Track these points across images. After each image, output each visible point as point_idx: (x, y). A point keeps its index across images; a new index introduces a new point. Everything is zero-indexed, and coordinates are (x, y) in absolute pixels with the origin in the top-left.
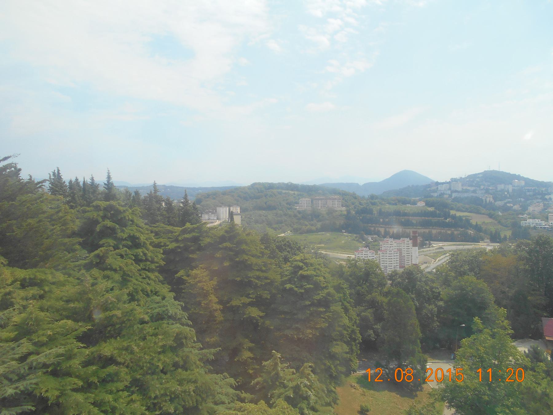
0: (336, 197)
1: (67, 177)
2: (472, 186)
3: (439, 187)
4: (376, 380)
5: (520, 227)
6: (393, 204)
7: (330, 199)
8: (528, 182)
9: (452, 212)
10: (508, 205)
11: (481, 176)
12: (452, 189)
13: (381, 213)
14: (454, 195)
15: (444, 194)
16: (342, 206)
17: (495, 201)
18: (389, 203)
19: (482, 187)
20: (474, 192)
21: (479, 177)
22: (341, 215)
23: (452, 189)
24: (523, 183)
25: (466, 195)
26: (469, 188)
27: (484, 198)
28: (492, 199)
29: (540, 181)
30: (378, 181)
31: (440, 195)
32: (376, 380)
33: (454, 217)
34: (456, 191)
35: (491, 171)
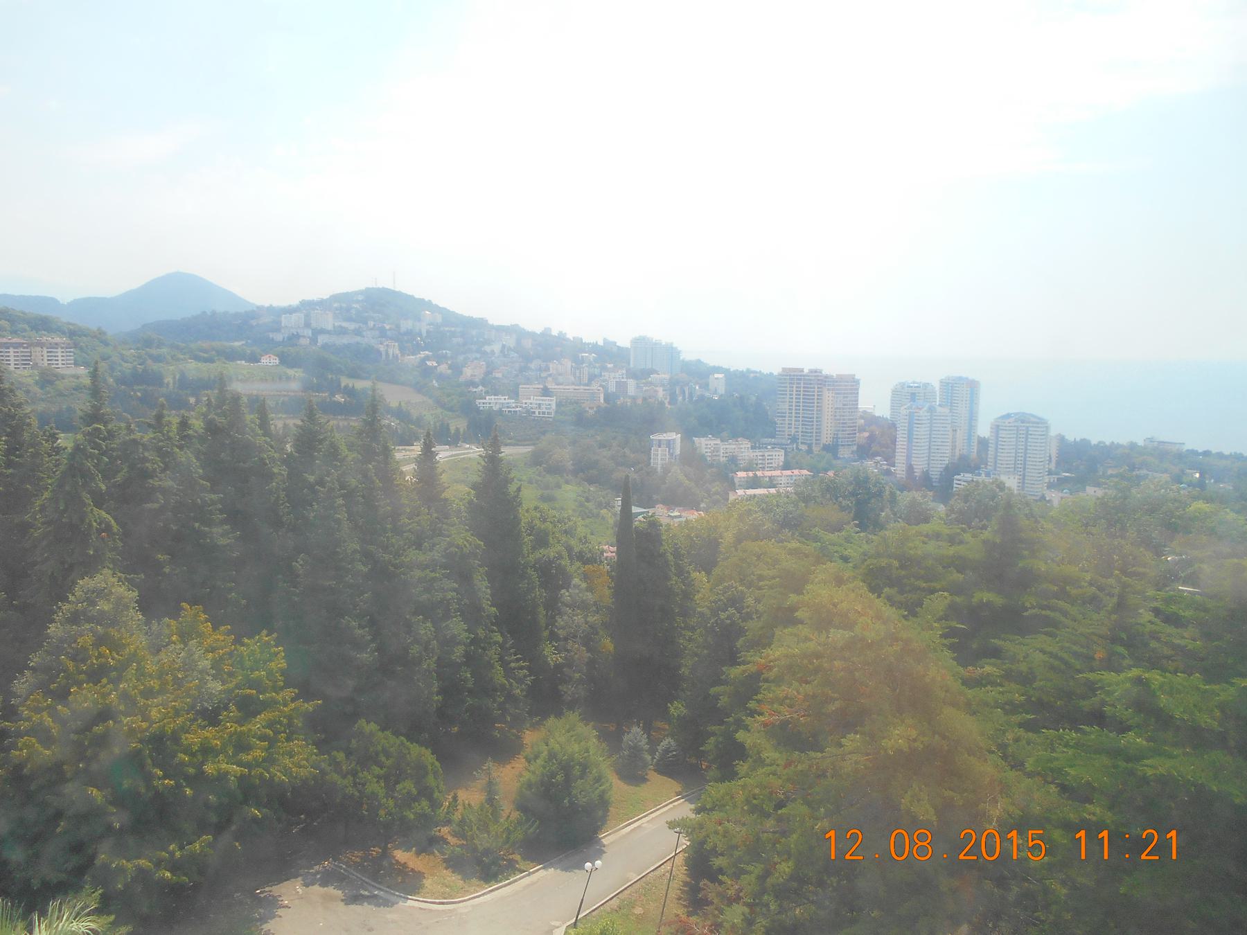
0: (57, 340)
1: (1070, 438)
2: (350, 320)
3: (284, 320)
4: (961, 857)
5: (478, 411)
6: (205, 360)
7: (41, 345)
8: (447, 315)
9: (345, 381)
10: (429, 363)
11: (360, 298)
12: (314, 325)
13: (183, 383)
14: (322, 339)
15: (298, 336)
16: (76, 364)
17: (403, 355)
18: (197, 358)
19: (371, 324)
20: (358, 332)
21: (358, 302)
22: (77, 388)
23: (314, 325)
24: (439, 319)
25: (345, 340)
26: (345, 324)
27: (382, 348)
28: (397, 352)
29: (466, 314)
30: (108, 296)
31: (289, 339)
32: (961, 857)
33: (350, 392)
34: (323, 331)
35: (379, 289)
